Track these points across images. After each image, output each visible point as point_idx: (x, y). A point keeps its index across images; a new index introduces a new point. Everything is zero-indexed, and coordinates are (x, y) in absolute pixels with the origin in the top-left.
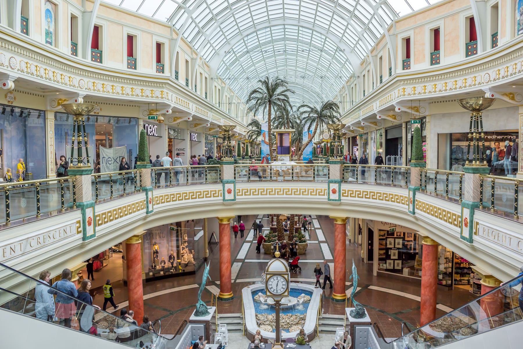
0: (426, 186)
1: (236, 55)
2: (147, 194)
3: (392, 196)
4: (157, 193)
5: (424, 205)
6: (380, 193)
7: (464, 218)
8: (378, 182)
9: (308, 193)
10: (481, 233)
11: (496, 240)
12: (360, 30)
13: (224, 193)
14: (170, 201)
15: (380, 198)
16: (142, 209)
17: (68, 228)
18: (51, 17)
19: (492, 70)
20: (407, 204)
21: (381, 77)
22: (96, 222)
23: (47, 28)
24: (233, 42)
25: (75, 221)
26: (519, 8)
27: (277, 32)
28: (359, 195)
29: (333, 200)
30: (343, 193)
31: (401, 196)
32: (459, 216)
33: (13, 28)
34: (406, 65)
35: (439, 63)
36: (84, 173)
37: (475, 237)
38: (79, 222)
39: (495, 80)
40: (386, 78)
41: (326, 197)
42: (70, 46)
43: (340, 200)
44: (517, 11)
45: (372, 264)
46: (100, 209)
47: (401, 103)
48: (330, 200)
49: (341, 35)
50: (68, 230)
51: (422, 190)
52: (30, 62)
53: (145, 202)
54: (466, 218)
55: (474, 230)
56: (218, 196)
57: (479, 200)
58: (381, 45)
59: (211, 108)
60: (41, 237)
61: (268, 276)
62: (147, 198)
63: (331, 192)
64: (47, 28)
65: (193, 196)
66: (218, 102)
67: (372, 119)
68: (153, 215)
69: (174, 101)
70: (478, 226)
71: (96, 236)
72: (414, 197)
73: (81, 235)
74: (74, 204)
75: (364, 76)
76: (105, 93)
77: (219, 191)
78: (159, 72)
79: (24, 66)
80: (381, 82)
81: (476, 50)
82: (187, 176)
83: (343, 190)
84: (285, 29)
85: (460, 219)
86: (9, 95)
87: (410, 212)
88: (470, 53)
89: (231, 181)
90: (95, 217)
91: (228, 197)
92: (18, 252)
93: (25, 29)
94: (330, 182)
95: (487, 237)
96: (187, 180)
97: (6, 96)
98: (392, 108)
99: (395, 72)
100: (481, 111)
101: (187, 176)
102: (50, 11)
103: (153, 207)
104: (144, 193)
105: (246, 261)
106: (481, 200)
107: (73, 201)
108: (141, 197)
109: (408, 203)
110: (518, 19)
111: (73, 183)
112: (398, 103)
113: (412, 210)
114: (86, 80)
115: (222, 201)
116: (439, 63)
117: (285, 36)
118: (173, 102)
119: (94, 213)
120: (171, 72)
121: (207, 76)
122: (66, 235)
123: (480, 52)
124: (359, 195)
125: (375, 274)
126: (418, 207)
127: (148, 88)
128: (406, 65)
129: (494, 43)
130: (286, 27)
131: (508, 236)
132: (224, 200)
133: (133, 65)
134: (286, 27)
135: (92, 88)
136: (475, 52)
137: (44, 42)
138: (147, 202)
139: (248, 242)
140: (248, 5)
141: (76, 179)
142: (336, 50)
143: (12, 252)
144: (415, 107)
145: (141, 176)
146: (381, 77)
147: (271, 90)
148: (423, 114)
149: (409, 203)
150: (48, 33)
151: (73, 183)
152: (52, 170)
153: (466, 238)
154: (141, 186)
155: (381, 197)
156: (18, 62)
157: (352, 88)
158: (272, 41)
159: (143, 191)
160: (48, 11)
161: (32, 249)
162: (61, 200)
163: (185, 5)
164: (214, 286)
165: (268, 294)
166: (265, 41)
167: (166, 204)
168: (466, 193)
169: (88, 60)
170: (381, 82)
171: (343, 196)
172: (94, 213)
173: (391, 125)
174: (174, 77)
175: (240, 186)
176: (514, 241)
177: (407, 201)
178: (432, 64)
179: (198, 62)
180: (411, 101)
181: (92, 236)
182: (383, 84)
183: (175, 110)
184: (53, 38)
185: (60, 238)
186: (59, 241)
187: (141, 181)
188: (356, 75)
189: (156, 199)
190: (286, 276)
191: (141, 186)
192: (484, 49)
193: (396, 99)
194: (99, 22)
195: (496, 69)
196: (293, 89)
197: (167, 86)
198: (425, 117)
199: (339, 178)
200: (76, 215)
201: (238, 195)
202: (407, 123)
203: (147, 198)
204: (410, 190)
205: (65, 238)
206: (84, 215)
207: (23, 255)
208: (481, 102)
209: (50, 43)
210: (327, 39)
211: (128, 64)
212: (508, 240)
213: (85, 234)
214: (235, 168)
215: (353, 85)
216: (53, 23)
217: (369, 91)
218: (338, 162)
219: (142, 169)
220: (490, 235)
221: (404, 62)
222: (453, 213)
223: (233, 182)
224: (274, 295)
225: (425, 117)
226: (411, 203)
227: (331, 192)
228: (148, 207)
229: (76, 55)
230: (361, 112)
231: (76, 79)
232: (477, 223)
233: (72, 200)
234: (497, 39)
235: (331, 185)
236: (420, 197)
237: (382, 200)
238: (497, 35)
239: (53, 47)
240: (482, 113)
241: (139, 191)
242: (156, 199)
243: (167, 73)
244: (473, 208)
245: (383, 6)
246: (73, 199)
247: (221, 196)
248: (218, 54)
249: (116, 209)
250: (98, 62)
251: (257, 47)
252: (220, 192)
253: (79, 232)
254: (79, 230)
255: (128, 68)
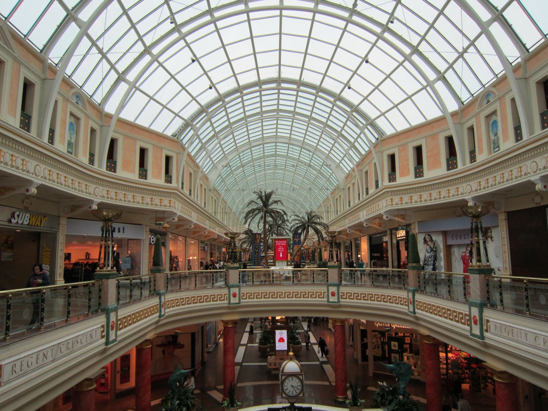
0: (425, 288)
1: (231, 169)
2: (160, 298)
3: (390, 298)
4: (169, 297)
5: (421, 304)
6: (385, 296)
7: (472, 316)
8: (375, 284)
9: (285, 296)
10: (492, 329)
11: (510, 336)
12: (346, 147)
13: (229, 297)
14: (185, 304)
15: (378, 299)
16: (156, 313)
17: (94, 332)
18: (73, 129)
19: (474, 182)
20: (406, 305)
21: (367, 189)
22: (117, 326)
23: (69, 139)
24: (230, 157)
25: (100, 325)
26: (492, 130)
27: (269, 149)
28: (357, 296)
29: (332, 302)
30: (342, 296)
31: (399, 297)
32: (466, 315)
33: (41, 139)
34: (392, 177)
35: (423, 176)
36: (111, 277)
37: (486, 334)
38: (103, 326)
39: (476, 190)
40: (372, 191)
41: (325, 299)
42: (88, 156)
43: (339, 302)
44: (491, 132)
45: (367, 365)
46: (123, 312)
47: (388, 212)
48: (330, 302)
49: (327, 152)
50: (94, 336)
51: (421, 291)
52: (53, 170)
53: (158, 306)
54: (475, 316)
55: (485, 328)
56: (224, 300)
57: (486, 299)
58: (367, 161)
59: (210, 218)
60: (70, 342)
61: (283, 377)
62: (160, 301)
63: (330, 295)
64: (69, 139)
65: (201, 299)
66: (214, 212)
67: (359, 227)
68: (165, 318)
69: (180, 210)
70: (489, 324)
71: (118, 340)
72: (414, 298)
73: (104, 340)
74: (99, 308)
75: (349, 188)
76: (118, 201)
77: (225, 295)
78: (168, 183)
79: (47, 172)
80: (367, 193)
81: (456, 164)
82: (196, 280)
83: (342, 293)
84: (276, 146)
85: (467, 318)
86: (26, 200)
87: (411, 312)
88: (450, 167)
89: (236, 285)
90: (117, 320)
91: (234, 300)
92: (50, 359)
93: (51, 139)
94: (328, 286)
95: (499, 333)
96: (196, 284)
97: (23, 202)
98: (380, 217)
99: (382, 184)
100: (481, 218)
101: (196, 280)
102: (73, 125)
103: (165, 311)
104: (158, 297)
105: (244, 364)
106: (488, 299)
107: (98, 305)
108: (155, 301)
109: (407, 304)
110: (493, 139)
111: (100, 287)
112: (386, 212)
113: (412, 310)
114: (101, 188)
115: (227, 305)
116: (423, 176)
117: (276, 152)
118: (179, 211)
119: (117, 317)
120: (178, 182)
121: (206, 188)
122: (92, 340)
123: (460, 166)
124: (357, 296)
125: (371, 374)
126: (418, 307)
127: (157, 197)
128: (392, 177)
129: (473, 158)
130: (278, 144)
131: (523, 332)
132: (229, 303)
133: (143, 174)
134: (278, 144)
135: (106, 196)
136: (455, 166)
137: (66, 152)
138: (160, 306)
139: (243, 345)
140: (262, 120)
141: (102, 283)
142: (322, 166)
143: (45, 358)
144: (401, 215)
145: (155, 281)
146: (367, 189)
147: (266, 199)
148: (408, 222)
149: (408, 303)
150: (70, 144)
151: (100, 287)
152: (60, 275)
153: (477, 335)
154: (155, 290)
155: (370, 297)
156: (42, 170)
157: (337, 199)
158: (264, 157)
159: (156, 295)
160: (71, 124)
161: (62, 354)
162: (98, 301)
163: (193, 122)
164: (215, 392)
165: (284, 395)
166: (259, 156)
167: (176, 308)
168: (472, 293)
169: (104, 169)
170: (367, 193)
171: (342, 298)
172: (117, 317)
173: (375, 232)
174: (180, 187)
175: (244, 290)
176: (531, 337)
177: (405, 302)
178: (416, 177)
179: (200, 175)
180: (398, 210)
181: (114, 341)
182: (368, 196)
183: (181, 219)
184: (74, 148)
185: (87, 343)
186: (85, 346)
187: (155, 285)
188: (342, 187)
189: (168, 303)
190: (301, 377)
191: (155, 290)
192: (464, 164)
193: (384, 209)
194: (116, 136)
195: (477, 181)
196: (283, 202)
197: (175, 196)
198: (410, 225)
199: (337, 281)
200: (100, 321)
201: (242, 299)
202: (391, 230)
203: (160, 301)
204: (408, 291)
205: (90, 344)
206: (108, 319)
207: (53, 361)
208: (479, 210)
209: (71, 153)
210: (314, 156)
211: (140, 174)
212: (523, 335)
213: (108, 339)
214: (239, 272)
215: (337, 197)
216: (75, 135)
217: (355, 202)
218: (336, 266)
219: (157, 274)
220: (503, 331)
221: (389, 175)
222: (459, 312)
223: (239, 287)
224: (290, 396)
225: (410, 225)
226: (411, 304)
227: (330, 295)
228: (160, 311)
229: (93, 165)
230: (347, 221)
231: (92, 188)
232: (488, 321)
233: (97, 304)
234: (475, 155)
235: (330, 288)
236: (419, 297)
237: (380, 301)
238: (475, 152)
239: (73, 156)
240: (481, 219)
241: (153, 294)
242: (168, 303)
243: (174, 184)
244: (481, 307)
245: (369, 127)
246: (98, 303)
247: (227, 300)
248: (216, 168)
249: (130, 315)
250: (112, 172)
251: (249, 162)
252: (226, 296)
253: (103, 337)
254: (103, 334)
255: (139, 178)
